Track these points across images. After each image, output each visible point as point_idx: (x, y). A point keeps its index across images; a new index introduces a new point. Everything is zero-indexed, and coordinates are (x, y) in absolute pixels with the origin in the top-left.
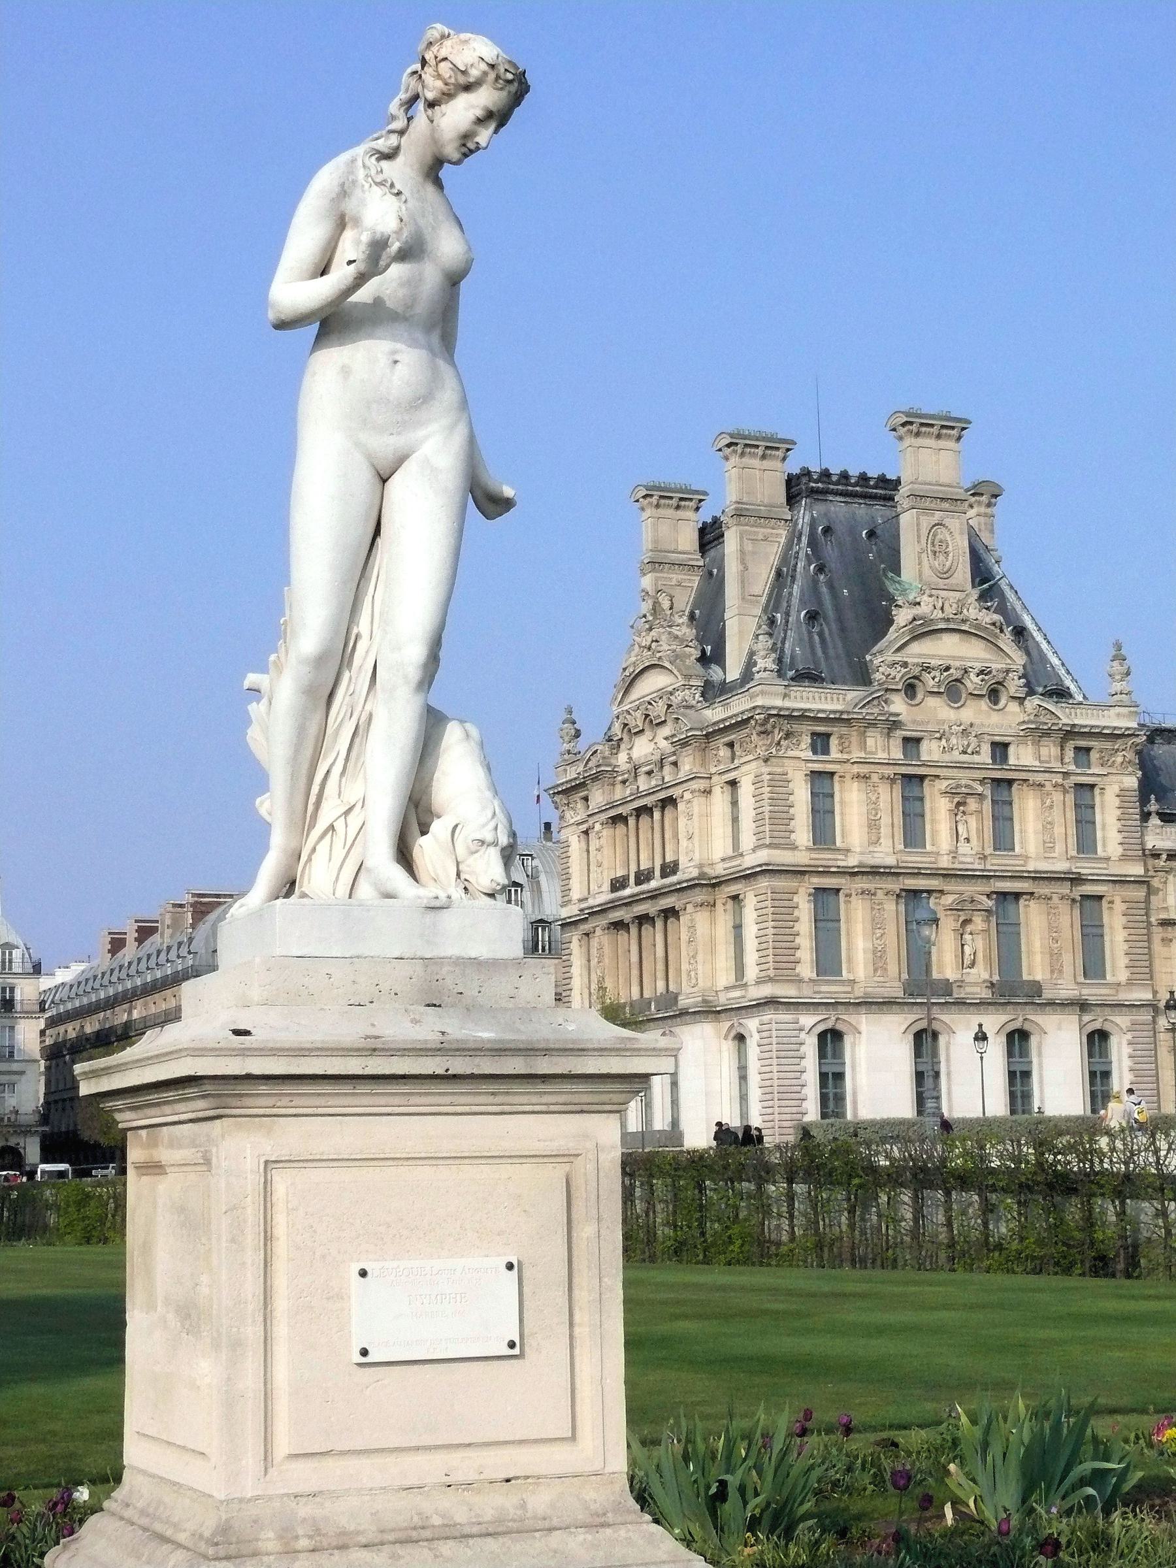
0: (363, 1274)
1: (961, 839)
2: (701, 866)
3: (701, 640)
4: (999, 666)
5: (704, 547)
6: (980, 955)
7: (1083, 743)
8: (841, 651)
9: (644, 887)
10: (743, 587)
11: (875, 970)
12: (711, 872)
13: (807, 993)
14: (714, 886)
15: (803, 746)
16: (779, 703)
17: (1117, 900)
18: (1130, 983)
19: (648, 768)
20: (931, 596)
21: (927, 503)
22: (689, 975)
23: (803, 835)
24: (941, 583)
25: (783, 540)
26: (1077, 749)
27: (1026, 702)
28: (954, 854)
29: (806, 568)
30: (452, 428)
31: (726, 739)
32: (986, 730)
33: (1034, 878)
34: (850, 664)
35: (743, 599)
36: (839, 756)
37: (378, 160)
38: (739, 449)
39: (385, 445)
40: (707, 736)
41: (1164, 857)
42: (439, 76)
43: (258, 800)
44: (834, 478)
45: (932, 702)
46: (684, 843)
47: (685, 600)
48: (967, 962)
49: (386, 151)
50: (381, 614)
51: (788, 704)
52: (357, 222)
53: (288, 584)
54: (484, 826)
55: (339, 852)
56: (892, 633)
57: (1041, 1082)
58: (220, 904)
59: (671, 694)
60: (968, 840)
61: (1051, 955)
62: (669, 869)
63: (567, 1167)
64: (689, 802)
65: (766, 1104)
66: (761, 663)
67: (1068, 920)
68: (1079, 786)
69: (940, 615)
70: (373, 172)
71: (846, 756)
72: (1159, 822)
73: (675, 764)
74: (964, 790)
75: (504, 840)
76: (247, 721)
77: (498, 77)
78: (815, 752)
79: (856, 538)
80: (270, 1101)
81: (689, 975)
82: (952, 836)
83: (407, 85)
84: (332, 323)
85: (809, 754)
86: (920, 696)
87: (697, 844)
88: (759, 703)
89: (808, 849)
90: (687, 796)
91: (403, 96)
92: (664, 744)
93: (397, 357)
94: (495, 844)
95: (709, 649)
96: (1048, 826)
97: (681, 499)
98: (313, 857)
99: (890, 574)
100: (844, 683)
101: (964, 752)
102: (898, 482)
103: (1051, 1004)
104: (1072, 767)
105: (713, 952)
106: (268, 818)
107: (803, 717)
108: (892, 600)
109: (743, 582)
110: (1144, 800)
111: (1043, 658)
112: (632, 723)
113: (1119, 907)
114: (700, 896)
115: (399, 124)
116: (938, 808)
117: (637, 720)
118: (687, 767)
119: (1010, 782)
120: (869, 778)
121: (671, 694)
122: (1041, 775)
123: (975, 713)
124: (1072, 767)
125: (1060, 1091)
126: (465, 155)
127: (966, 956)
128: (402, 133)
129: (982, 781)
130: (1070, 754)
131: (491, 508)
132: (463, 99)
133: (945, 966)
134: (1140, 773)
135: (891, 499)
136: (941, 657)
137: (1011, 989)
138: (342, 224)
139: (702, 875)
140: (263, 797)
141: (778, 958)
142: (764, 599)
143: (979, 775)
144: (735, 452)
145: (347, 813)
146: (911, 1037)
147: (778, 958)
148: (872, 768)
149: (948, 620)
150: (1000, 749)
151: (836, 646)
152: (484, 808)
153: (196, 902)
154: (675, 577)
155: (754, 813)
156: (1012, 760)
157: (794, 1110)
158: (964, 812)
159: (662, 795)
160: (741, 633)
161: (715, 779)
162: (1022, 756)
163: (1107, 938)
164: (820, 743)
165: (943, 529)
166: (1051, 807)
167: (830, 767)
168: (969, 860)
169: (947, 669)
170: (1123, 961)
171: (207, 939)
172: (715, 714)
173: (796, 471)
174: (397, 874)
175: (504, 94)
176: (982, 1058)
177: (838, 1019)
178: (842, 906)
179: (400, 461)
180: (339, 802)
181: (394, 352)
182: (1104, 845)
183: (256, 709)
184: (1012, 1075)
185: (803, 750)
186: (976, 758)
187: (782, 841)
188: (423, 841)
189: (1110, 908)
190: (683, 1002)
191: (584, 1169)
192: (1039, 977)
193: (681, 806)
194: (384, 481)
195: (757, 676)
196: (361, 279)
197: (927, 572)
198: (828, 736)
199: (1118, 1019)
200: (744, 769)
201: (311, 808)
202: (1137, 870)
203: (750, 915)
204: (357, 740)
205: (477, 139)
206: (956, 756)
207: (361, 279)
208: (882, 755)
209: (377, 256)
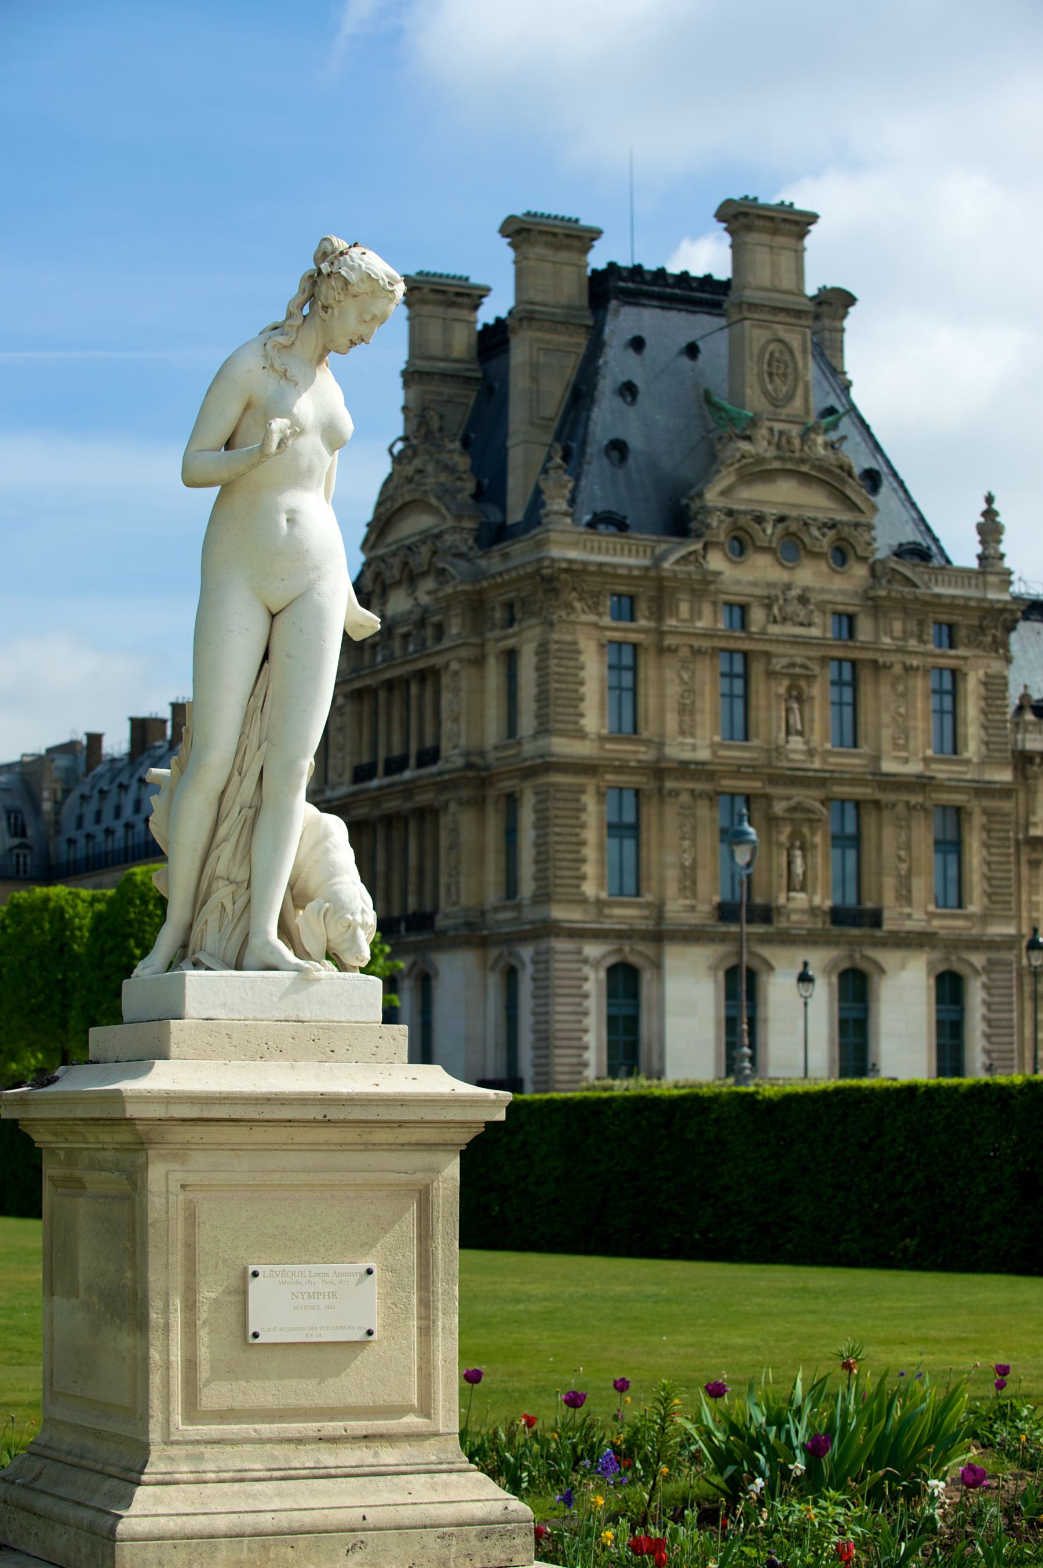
0: (369, 1272)
2: (467, 754)
3: (476, 470)
9: (396, 778)
17: (977, 811)
26: (939, 624)
31: (505, 598)
46: (447, 726)
57: (561, 403)
62: (430, 756)
64: (456, 673)
65: (539, 1052)
74: (798, 670)
81: (448, 890)
82: (808, 739)
85: (607, 621)
87: (463, 726)
90: (454, 666)
95: (486, 481)
96: (620, 584)
105: (480, 861)
116: (768, 695)
117: (394, 572)
122: (892, 655)
124: (931, 647)
125: (904, 1054)
130: (931, 630)
135: (718, 305)
136: (775, 504)
142: (555, 424)
146: (721, 975)
150: (848, 622)
157: (574, 1060)
164: (851, 841)
173: (601, 266)
176: (806, 1004)
184: (843, 1023)
190: (440, 922)
193: (445, 680)
202: (1005, 776)
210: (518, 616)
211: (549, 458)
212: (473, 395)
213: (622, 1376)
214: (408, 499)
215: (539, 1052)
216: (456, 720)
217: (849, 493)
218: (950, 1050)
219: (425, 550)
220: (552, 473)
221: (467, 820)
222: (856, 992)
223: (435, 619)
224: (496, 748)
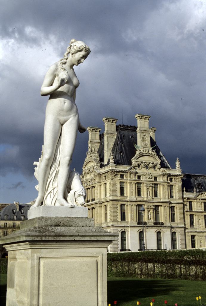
1: (148, 195)
4: (156, 162)
5: (100, 139)
6: (152, 217)
7: (171, 177)
8: (126, 159)
9: (88, 203)
10: (108, 147)
11: (132, 220)
12: (101, 201)
13: (119, 224)
14: (101, 203)
15: (119, 177)
16: (114, 169)
18: (180, 223)
19: (89, 181)
20: (143, 149)
21: (142, 131)
22: (96, 220)
23: (119, 194)
24: (145, 147)
25: (115, 138)
26: (170, 178)
27: (161, 169)
28: (147, 198)
29: (120, 143)
30: (75, 115)
32: (153, 174)
33: (145, 202)
34: (128, 161)
35: (108, 149)
36: (125, 179)
37: (62, 64)
38: (107, 121)
39: (62, 118)
40: (101, 174)
41: (186, 199)
42: (74, 49)
43: (36, 186)
44: (122, 126)
45: (143, 169)
47: (97, 149)
48: (149, 218)
49: (64, 62)
50: (61, 151)
51: (116, 169)
52: (58, 75)
53: (43, 144)
54: (80, 192)
55: (52, 197)
56: (136, 156)
58: (6, 206)
59: (94, 166)
60: (150, 195)
61: (165, 217)
63: (96, 258)
64: (97, 187)
66: (111, 161)
67: (167, 209)
68: (170, 185)
69: (145, 152)
70: (61, 66)
71: (127, 179)
72: (185, 192)
73: (95, 180)
75: (84, 195)
76: (34, 171)
77: (85, 49)
78: (121, 178)
79: (129, 138)
80: (40, 246)
81: (96, 220)
83: (68, 50)
84: (53, 95)
85: (120, 178)
86: (141, 168)
88: (111, 169)
89: (120, 196)
90: (97, 186)
91: (67, 52)
92: (92, 176)
93: (65, 102)
94: (83, 195)
97: (96, 130)
98: (47, 198)
99: (135, 145)
100: (127, 165)
101: (149, 178)
102: (137, 127)
103: (165, 227)
104: (169, 182)
106: (38, 190)
107: (119, 171)
108: (136, 149)
109: (108, 146)
110: (182, 189)
111: (164, 161)
112: (86, 172)
113: (178, 208)
114: (98, 205)
115: (66, 57)
118: (97, 180)
119: (158, 184)
120: (131, 183)
121: (94, 166)
123: (151, 171)
124: (169, 182)
125: (166, 244)
126: (79, 64)
127: (149, 217)
128: (67, 59)
129: (152, 184)
130: (169, 179)
131: (82, 131)
132: (79, 53)
133: (145, 219)
134: (182, 183)
136: (145, 160)
137: (157, 223)
138: (55, 76)
139: (99, 201)
140: (37, 185)
141: (114, 217)
142: (112, 149)
143: (152, 183)
144: (107, 121)
145: (54, 189)
146: (138, 233)
147: (114, 217)
148: (132, 181)
149: (146, 153)
150: (156, 178)
151: (125, 158)
152: (81, 188)
153: (1, 206)
154: (95, 144)
155: (109, 189)
156: (158, 180)
158: (149, 190)
159: (92, 186)
160: (107, 155)
161: (102, 183)
162: (160, 179)
163: (160, 214)
164: (122, 176)
165: (145, 136)
166: (165, 189)
167: (124, 181)
168: (150, 199)
169: (146, 163)
170: (179, 219)
171: (3, 212)
172: (102, 171)
174: (64, 201)
175: (86, 53)
177: (125, 229)
178: (126, 207)
179: (65, 121)
180: (52, 187)
181: (65, 101)
182: (175, 196)
183: (35, 168)
185: (119, 177)
186: (151, 180)
187: (115, 195)
188: (69, 194)
189: (177, 209)
191: (99, 259)
192: (163, 222)
193: (96, 188)
194: (62, 125)
195: (110, 163)
196: (59, 87)
197: (142, 144)
198: (123, 175)
199: (178, 230)
200: (108, 181)
201: (47, 188)
203: (108, 209)
204: (55, 180)
205: (81, 61)
206: (147, 179)
207: (59, 87)
208: (134, 179)
209: (62, 82)
210: (106, 178)
211: (111, 154)
212: (99, 145)
213: (91, 51)
214: (89, 161)
215: (111, 248)
216: (97, 194)
217: (156, 158)
218: (174, 246)
219: (92, 168)
220: (111, 156)
221: (99, 209)
222: (159, 233)
223: (94, 179)
224: (103, 198)
